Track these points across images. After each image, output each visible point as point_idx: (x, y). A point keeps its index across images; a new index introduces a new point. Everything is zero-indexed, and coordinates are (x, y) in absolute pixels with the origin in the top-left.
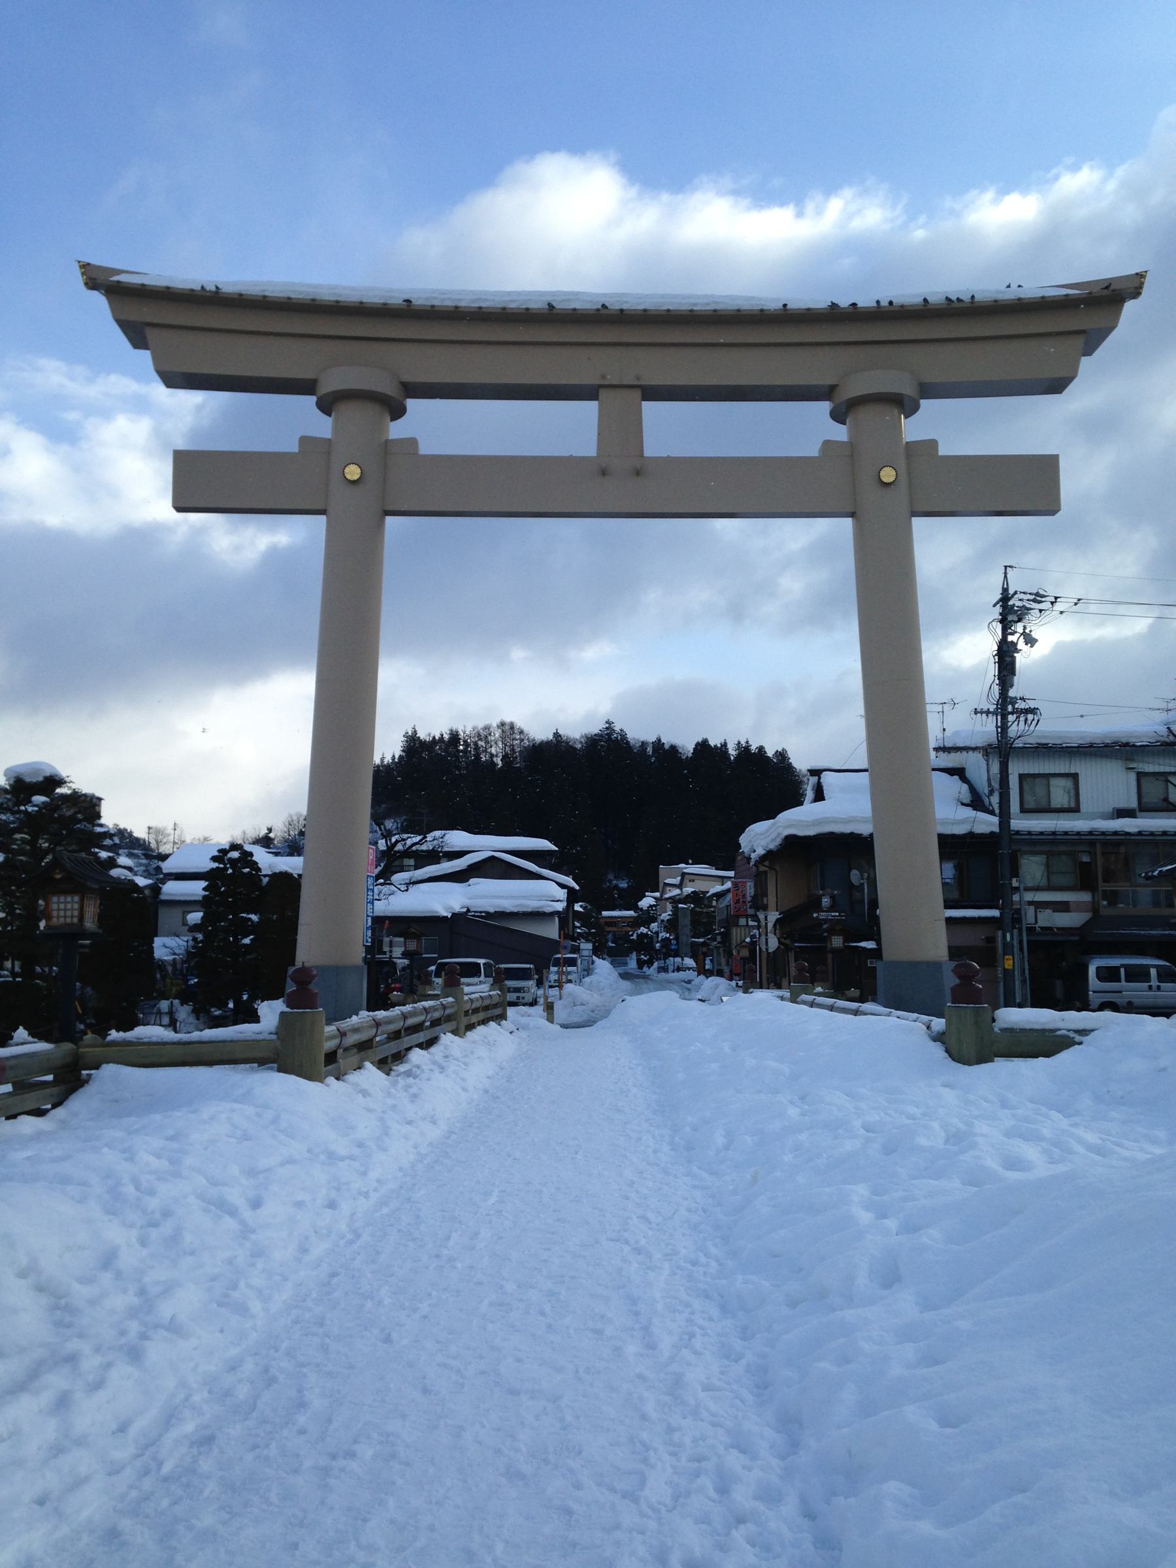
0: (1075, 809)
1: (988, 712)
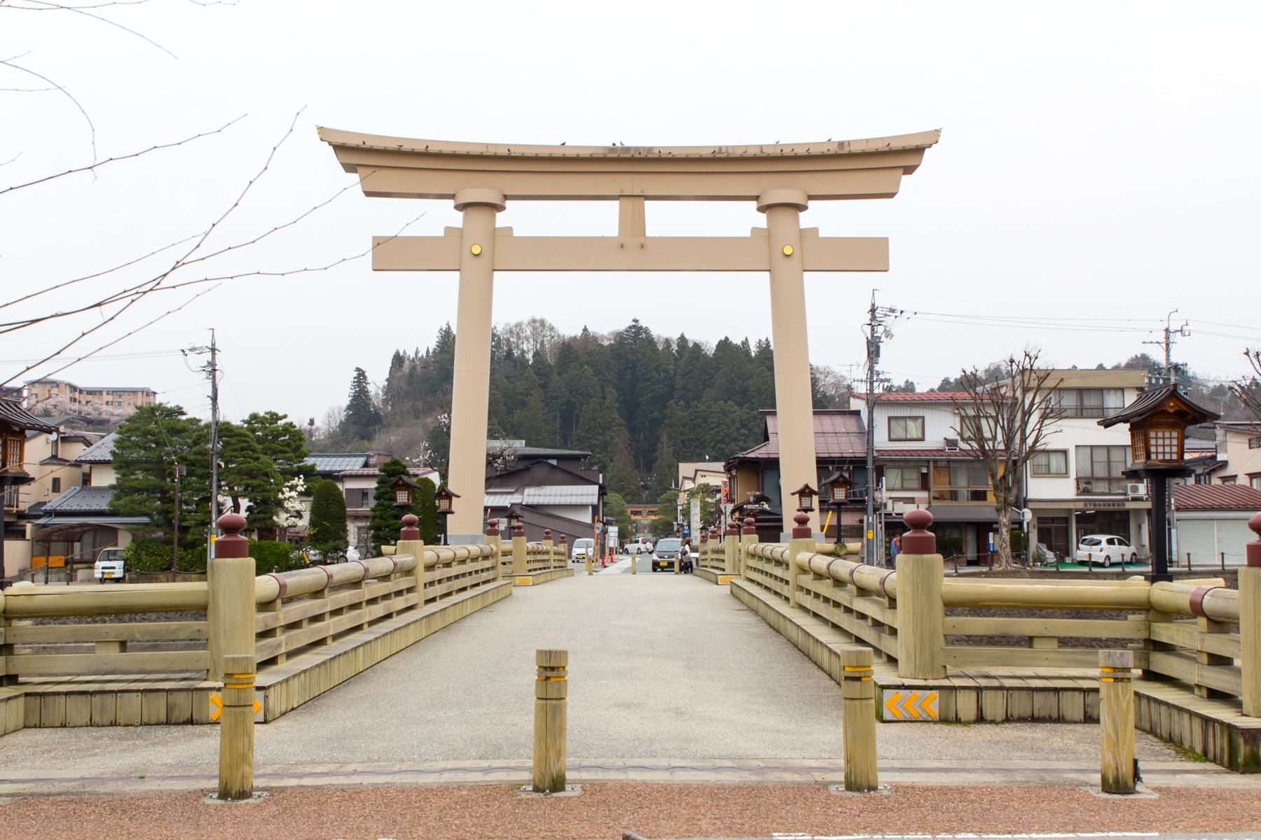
0: (922, 439)
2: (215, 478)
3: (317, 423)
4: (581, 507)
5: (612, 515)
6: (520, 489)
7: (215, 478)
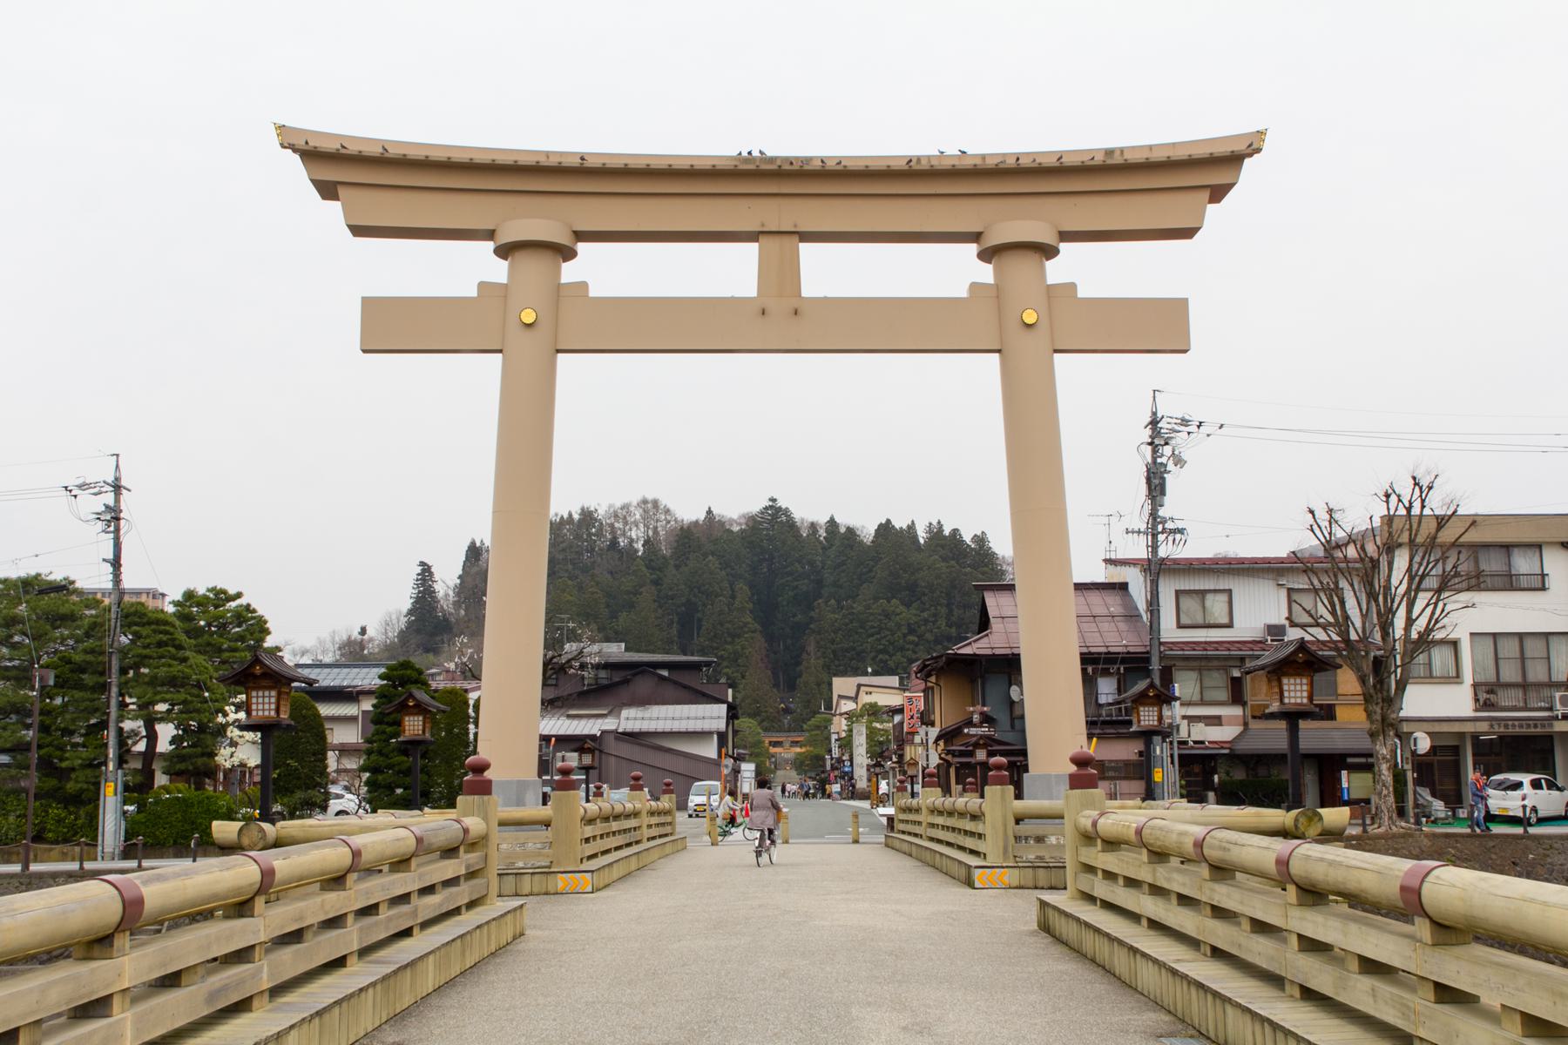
0: (1230, 625)
1: (1139, 532)
2: (114, 690)
3: (371, 632)
4: (702, 735)
5: (745, 747)
6: (614, 711)
7: (114, 690)
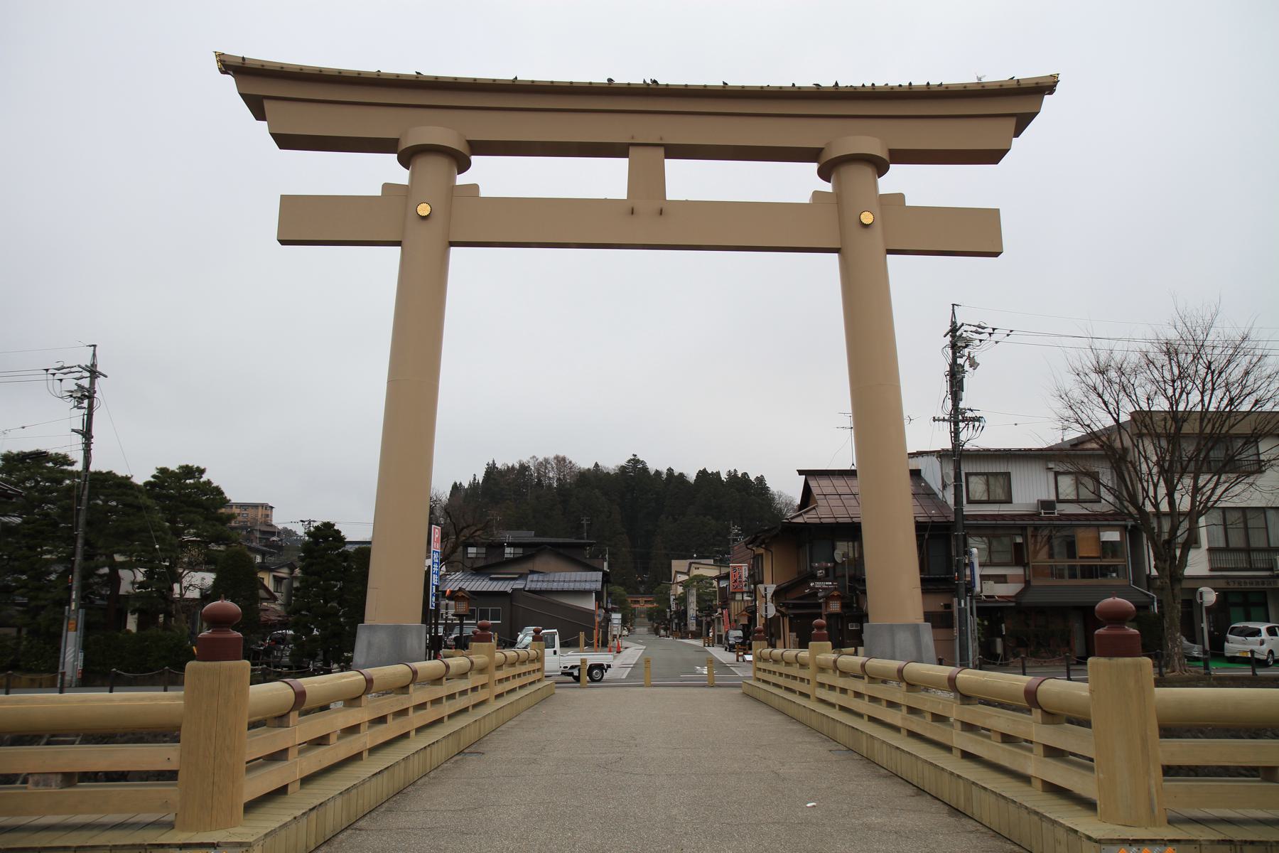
0: (1009, 501)
4: (584, 593)
6: (522, 576)
